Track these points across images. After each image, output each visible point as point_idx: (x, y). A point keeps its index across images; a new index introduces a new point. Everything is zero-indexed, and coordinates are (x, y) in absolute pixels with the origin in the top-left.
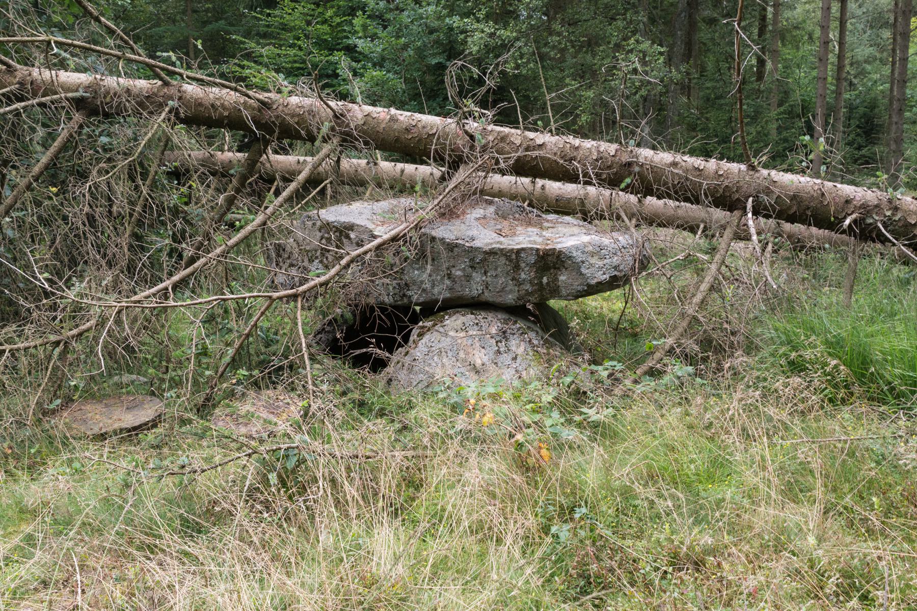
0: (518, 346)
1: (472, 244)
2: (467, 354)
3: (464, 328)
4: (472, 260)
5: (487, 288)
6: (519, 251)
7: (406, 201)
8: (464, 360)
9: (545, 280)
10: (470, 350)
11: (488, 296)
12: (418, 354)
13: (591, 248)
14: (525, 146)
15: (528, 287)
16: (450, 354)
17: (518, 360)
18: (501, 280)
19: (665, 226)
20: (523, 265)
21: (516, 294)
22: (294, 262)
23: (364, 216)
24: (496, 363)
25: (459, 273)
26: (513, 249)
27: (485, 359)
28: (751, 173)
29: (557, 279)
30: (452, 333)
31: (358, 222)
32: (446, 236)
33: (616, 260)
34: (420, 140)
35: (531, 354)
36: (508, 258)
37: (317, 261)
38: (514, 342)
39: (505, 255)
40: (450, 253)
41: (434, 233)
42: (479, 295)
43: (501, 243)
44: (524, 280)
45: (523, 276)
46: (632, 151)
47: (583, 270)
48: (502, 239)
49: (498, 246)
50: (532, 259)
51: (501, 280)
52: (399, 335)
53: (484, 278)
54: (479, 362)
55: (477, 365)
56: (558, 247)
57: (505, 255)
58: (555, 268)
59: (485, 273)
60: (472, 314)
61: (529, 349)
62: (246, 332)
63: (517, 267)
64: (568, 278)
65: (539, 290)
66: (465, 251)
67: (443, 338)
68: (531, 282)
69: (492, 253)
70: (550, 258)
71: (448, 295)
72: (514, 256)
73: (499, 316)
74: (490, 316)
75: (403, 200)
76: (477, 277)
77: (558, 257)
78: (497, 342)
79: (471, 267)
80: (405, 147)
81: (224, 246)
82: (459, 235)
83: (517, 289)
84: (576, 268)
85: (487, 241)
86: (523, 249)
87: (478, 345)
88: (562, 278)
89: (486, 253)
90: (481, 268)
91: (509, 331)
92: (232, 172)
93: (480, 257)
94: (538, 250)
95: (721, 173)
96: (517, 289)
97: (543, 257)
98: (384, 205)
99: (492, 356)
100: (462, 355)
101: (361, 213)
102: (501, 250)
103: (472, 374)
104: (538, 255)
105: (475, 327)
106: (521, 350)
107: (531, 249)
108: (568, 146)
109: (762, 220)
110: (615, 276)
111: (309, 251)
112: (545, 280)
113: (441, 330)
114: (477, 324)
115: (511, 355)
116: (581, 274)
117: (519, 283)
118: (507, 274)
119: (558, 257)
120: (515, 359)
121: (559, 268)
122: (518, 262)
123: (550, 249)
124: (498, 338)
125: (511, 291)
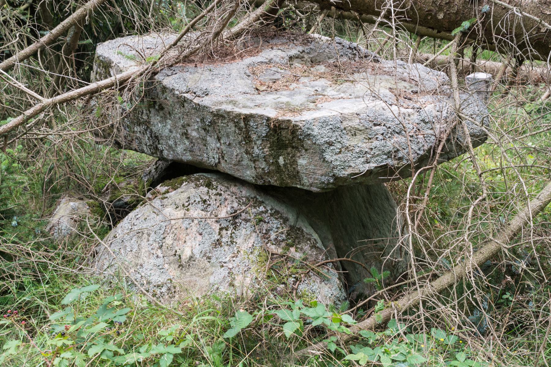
2: (176, 239)
4: (202, 120)
10: (182, 236)
13: (355, 123)
16: (153, 237)
20: (254, 137)
26: (240, 115)
29: (294, 162)
32: (176, 86)
33: (391, 144)
36: (237, 125)
38: (244, 230)
44: (258, 156)
47: (328, 156)
50: (263, 130)
55: (183, 257)
59: (219, 139)
64: (310, 164)
78: (221, 229)
86: (251, 116)
87: (195, 229)
88: (302, 162)
94: (268, 119)
99: (207, 247)
100: (169, 241)
109: (93, 75)
110: (386, 166)
114: (205, 201)
121: (297, 148)
122: (248, 131)
123: (283, 121)
125: (248, 167)
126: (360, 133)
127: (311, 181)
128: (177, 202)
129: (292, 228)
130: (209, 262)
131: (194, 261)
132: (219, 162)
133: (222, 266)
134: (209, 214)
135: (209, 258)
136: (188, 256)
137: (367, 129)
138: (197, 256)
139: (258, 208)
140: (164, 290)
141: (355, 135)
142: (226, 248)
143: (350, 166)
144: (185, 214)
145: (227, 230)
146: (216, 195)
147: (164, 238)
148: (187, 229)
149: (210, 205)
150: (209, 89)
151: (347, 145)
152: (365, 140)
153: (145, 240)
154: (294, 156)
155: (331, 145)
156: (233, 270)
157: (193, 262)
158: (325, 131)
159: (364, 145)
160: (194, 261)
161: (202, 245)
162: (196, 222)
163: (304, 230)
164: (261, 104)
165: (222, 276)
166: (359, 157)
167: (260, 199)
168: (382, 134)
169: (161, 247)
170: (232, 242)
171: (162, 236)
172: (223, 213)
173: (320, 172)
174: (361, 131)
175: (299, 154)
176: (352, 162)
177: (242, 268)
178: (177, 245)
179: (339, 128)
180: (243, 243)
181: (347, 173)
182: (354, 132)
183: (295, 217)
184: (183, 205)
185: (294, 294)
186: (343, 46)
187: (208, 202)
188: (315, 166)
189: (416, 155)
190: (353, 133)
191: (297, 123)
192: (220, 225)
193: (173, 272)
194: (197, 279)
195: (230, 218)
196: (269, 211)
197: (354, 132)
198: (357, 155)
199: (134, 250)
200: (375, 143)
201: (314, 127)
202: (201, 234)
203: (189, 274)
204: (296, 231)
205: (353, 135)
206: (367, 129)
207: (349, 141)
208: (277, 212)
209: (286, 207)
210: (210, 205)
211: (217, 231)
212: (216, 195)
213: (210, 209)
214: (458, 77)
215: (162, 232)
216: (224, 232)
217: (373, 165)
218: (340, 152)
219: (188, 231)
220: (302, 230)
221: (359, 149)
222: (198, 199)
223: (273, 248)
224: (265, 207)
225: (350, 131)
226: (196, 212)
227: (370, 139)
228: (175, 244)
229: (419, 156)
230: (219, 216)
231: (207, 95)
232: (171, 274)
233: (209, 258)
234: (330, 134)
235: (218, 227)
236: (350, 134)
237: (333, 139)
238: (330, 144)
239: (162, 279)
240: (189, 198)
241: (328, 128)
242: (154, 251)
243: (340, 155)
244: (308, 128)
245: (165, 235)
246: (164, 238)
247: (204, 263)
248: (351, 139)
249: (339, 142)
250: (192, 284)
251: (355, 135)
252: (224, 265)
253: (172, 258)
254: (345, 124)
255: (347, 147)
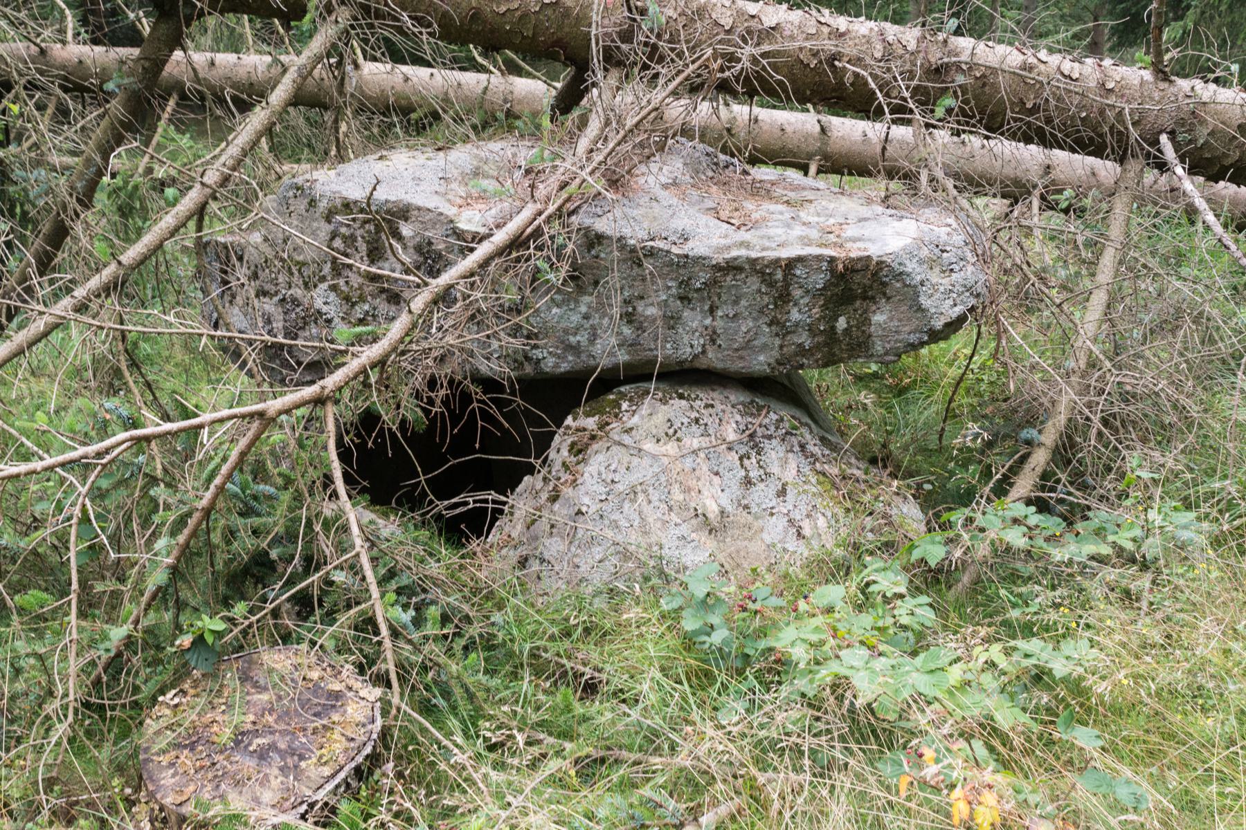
0: (784, 463)
1: (686, 249)
3: (673, 435)
5: (713, 341)
6: (791, 263)
7: (498, 148)
8: (684, 507)
9: (842, 323)
10: (692, 483)
11: (714, 358)
12: (586, 500)
14: (740, 29)
15: (804, 339)
17: (791, 495)
18: (746, 325)
19: (870, 174)
20: (797, 293)
21: (775, 354)
22: (267, 287)
23: (424, 186)
24: (746, 507)
25: (652, 311)
26: (778, 260)
27: (725, 501)
28: (1163, 85)
29: (867, 321)
30: (649, 446)
31: (418, 200)
32: (627, 232)
34: (525, 16)
35: (814, 480)
37: (324, 286)
39: (762, 273)
40: (636, 270)
41: (602, 226)
42: (696, 356)
43: (744, 244)
44: (797, 324)
45: (795, 315)
46: (945, 41)
47: (925, 302)
48: (743, 235)
49: (743, 252)
50: (819, 280)
51: (746, 325)
52: (537, 458)
53: (708, 321)
54: (712, 509)
55: (711, 516)
56: (874, 251)
57: (762, 273)
58: (865, 298)
59: (712, 310)
60: (681, 397)
61: (806, 470)
62: (204, 503)
63: (784, 298)
64: (891, 319)
65: (826, 344)
66: (671, 263)
67: (636, 460)
68: (812, 330)
69: (732, 267)
70: (857, 278)
71: (627, 357)
72: (779, 275)
73: (732, 398)
74: (716, 396)
75: (495, 146)
76: (694, 319)
77: (875, 274)
78: (741, 459)
79: (682, 298)
80: (492, 31)
81: (113, 267)
82: (655, 228)
83: (778, 342)
84: (910, 296)
85: (716, 241)
86: (800, 259)
87: (705, 468)
88: (878, 318)
89: (717, 268)
90: (702, 300)
91: (760, 431)
92: (110, 86)
93: (704, 277)
94: (832, 260)
95: (1110, 85)
96: (778, 342)
97: (842, 276)
98: (462, 156)
99: (735, 490)
101: (418, 180)
102: (753, 262)
103: (703, 536)
104: (832, 270)
105: (694, 428)
106: (790, 474)
107: (819, 258)
108: (825, 30)
111: (303, 264)
112: (842, 323)
113: (627, 439)
115: (774, 486)
116: (920, 309)
117: (781, 327)
118: (761, 312)
119: (875, 274)
120: (782, 493)
121: (873, 298)
122: (787, 285)
124: (743, 450)
125: (764, 347)
127: (888, 346)
128: (654, 432)
132: (704, 352)
133: (772, 514)
138: (729, 509)
145: (749, 458)
150: (688, 229)
154: (865, 311)
156: (792, 516)
161: (727, 490)
162: (702, 455)
165: (780, 528)
167: (761, 403)
173: (907, 329)
175: (874, 308)
177: (804, 509)
184: (667, 434)
188: (900, 320)
191: (884, 259)
198: (942, 297)
199: (636, 524)
202: (717, 474)
214: (449, 264)
219: (697, 473)
226: (693, 441)
231: (686, 240)
233: (746, 507)
244: (900, 264)
247: (743, 517)
250: (742, 553)
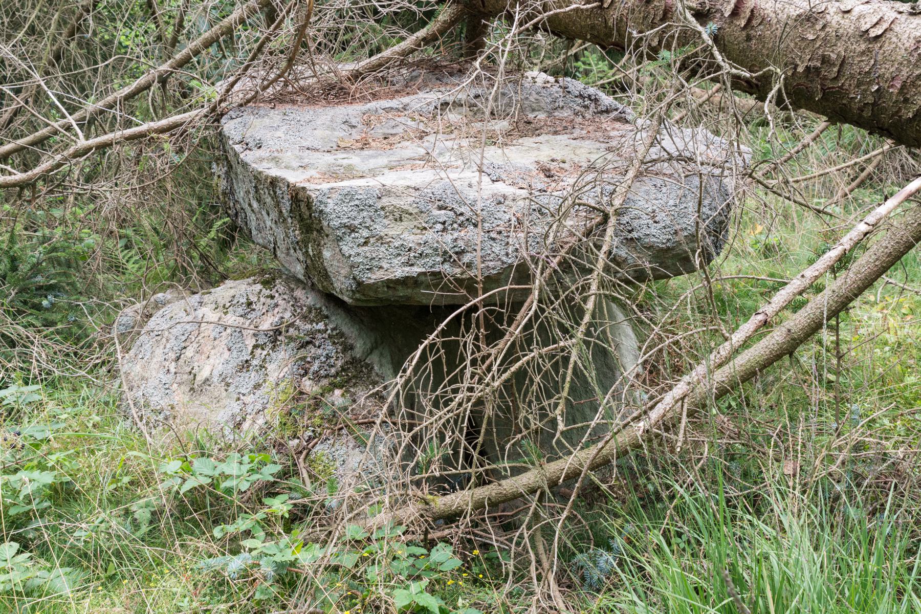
13: (404, 203)
55: (198, 378)
78: (256, 347)
99: (230, 369)
100: (189, 353)
126: (410, 217)
129: (354, 362)
130: (226, 390)
131: (210, 385)
134: (248, 322)
135: (228, 385)
136: (204, 378)
137: (422, 212)
138: (215, 379)
139: (314, 324)
140: (161, 417)
141: (401, 220)
142: (253, 374)
143: (381, 267)
144: (220, 318)
145: (263, 349)
146: (267, 297)
147: (185, 348)
148: (215, 339)
149: (254, 310)
151: (382, 234)
152: (415, 231)
153: (162, 347)
155: (353, 231)
157: (208, 387)
158: (345, 209)
159: (412, 237)
160: (210, 385)
163: (376, 368)
164: (307, 166)
166: (399, 255)
168: (444, 223)
169: (178, 358)
170: (262, 367)
171: (183, 345)
172: (267, 324)
174: (411, 214)
176: (386, 261)
178: (198, 361)
179: (370, 206)
180: (275, 371)
181: (374, 277)
182: (400, 216)
183: (369, 345)
184: (224, 305)
185: (303, 456)
186: (569, 92)
187: (254, 307)
189: (499, 263)
190: (397, 216)
192: (257, 341)
193: (180, 396)
194: (205, 411)
195: (272, 333)
196: (329, 331)
197: (400, 216)
198: (396, 252)
200: (430, 235)
201: (329, 200)
203: (198, 402)
204: (362, 367)
205: (396, 220)
206: (422, 212)
207: (393, 230)
208: (342, 335)
209: (361, 329)
210: (254, 310)
211: (250, 348)
212: (267, 297)
213: (252, 316)
215: (184, 338)
216: (259, 351)
217: (416, 270)
218: (366, 243)
219: (216, 342)
220: (372, 368)
221: (400, 242)
222: (244, 300)
223: (308, 385)
224: (326, 325)
225: (392, 212)
227: (425, 228)
228: (196, 358)
229: (506, 266)
230: (260, 328)
232: (177, 398)
234: (354, 214)
235: (253, 342)
236: (391, 217)
237: (356, 223)
238: (352, 229)
239: (164, 403)
240: (234, 297)
241: (352, 203)
242: (167, 364)
243: (366, 248)
245: (187, 344)
246: (185, 348)
248: (392, 225)
249: (367, 228)
251: (401, 220)
252: (242, 397)
253: (186, 376)
254: (385, 201)
255: (381, 238)
